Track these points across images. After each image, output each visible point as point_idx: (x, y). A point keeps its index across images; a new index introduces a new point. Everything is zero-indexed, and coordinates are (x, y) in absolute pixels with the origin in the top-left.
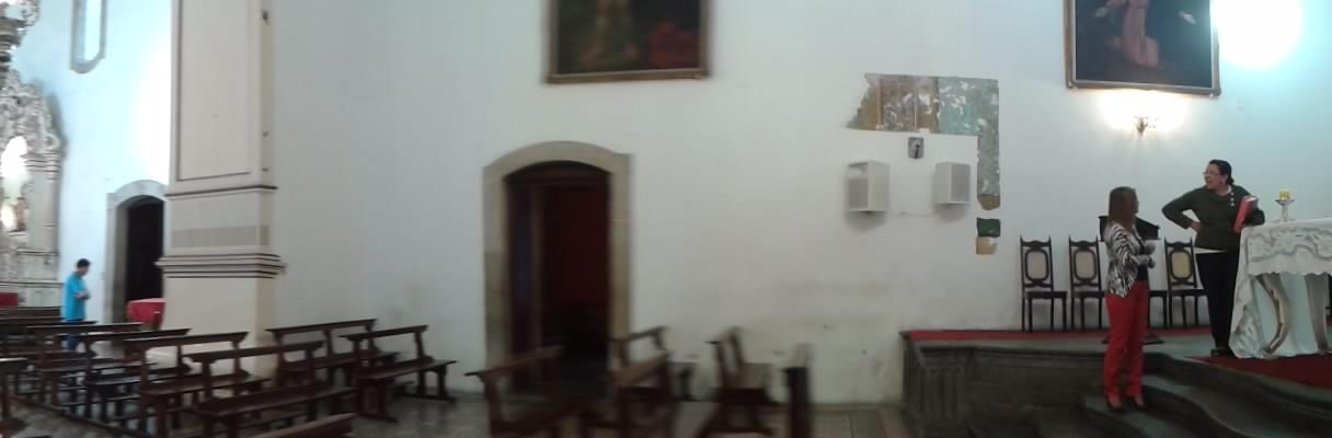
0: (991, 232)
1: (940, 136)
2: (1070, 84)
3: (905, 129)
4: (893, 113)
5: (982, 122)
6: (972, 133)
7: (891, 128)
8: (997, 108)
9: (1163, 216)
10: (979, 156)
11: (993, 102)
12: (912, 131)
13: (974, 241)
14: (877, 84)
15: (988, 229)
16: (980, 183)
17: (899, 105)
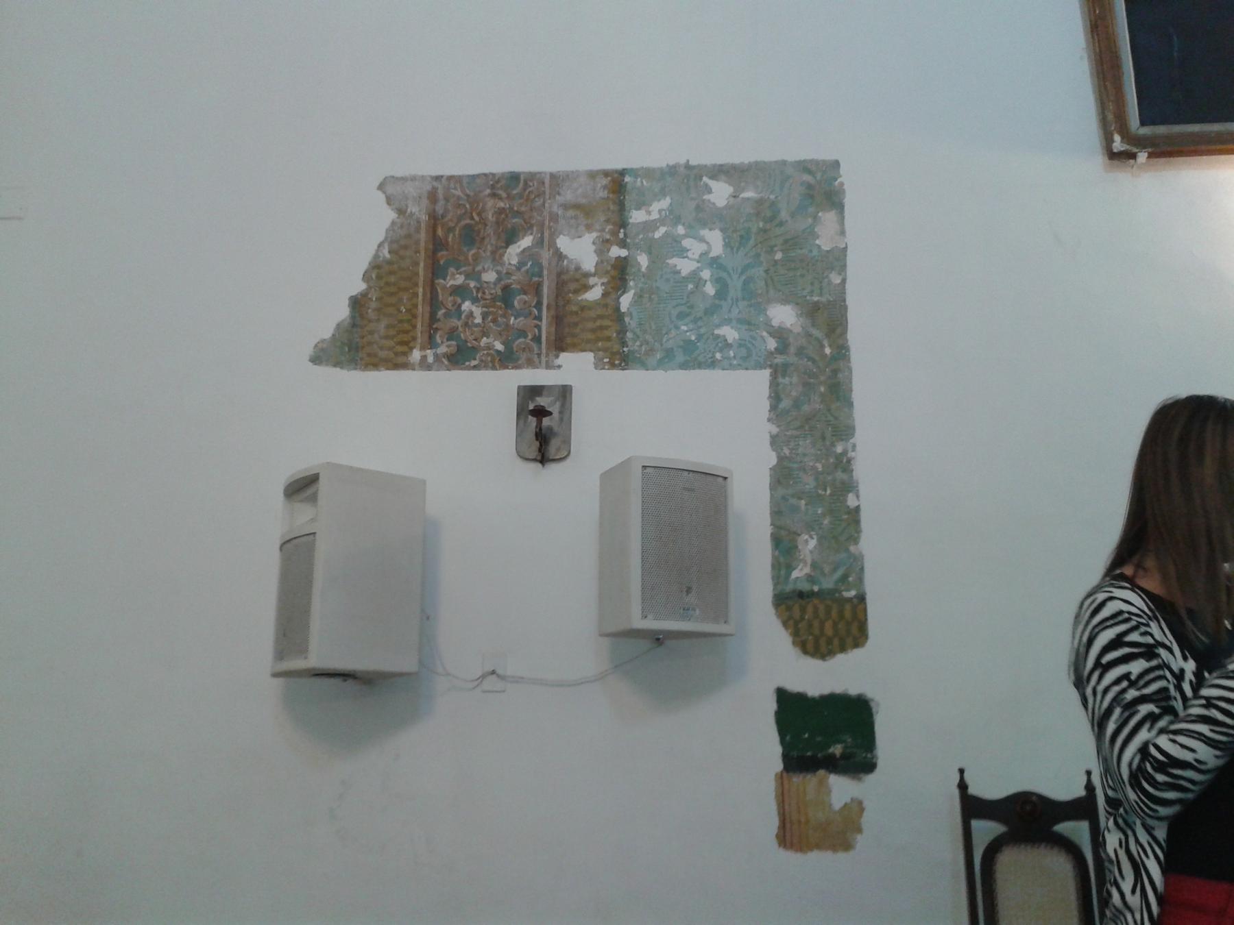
0: (837, 750)
1: (633, 376)
2: (1118, 144)
3: (506, 360)
4: (467, 306)
5: (784, 315)
6: (747, 359)
7: (459, 358)
8: (838, 260)
9: (854, 689)
10: (775, 441)
11: (825, 241)
12: (530, 364)
13: (768, 787)
14: (418, 211)
15: (827, 736)
16: (784, 546)
17: (490, 277)
